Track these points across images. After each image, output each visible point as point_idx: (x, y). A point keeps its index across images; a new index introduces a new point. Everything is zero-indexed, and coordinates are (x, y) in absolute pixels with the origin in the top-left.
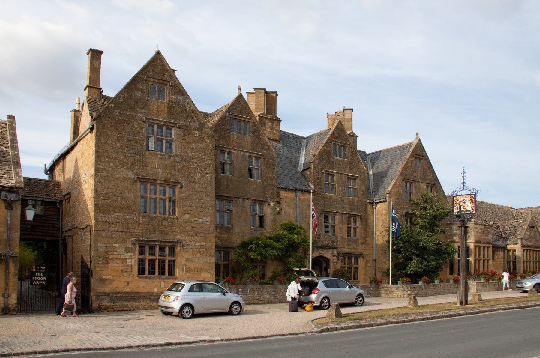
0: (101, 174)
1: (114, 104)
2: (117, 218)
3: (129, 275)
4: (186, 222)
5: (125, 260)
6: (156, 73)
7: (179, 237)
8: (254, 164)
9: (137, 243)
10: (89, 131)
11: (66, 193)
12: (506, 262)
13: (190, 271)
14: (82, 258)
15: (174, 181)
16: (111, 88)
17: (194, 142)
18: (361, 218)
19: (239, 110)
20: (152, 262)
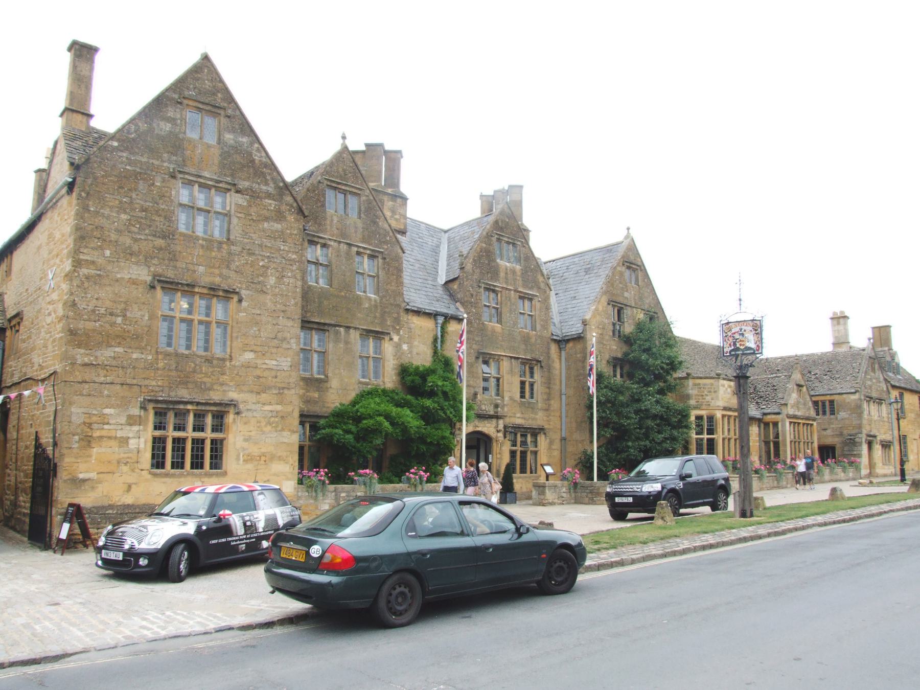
0: (84, 271)
1: (118, 140)
2: (114, 358)
3: (133, 471)
4: (247, 366)
5: (124, 441)
6: (201, 90)
7: (233, 395)
8: (366, 266)
9: (150, 406)
10: (64, 191)
11: (14, 313)
12: (763, 443)
13: (251, 460)
14: (37, 439)
15: (226, 288)
16: (111, 113)
17: (267, 219)
18: (541, 367)
19: (342, 173)
20: (179, 443)
